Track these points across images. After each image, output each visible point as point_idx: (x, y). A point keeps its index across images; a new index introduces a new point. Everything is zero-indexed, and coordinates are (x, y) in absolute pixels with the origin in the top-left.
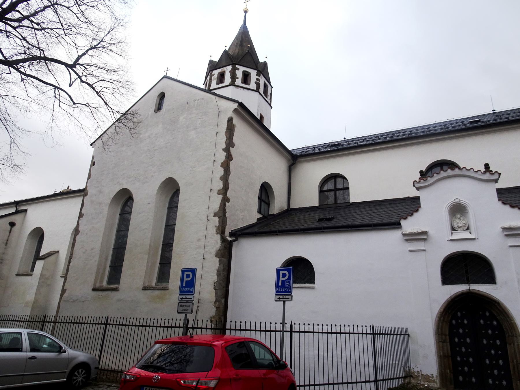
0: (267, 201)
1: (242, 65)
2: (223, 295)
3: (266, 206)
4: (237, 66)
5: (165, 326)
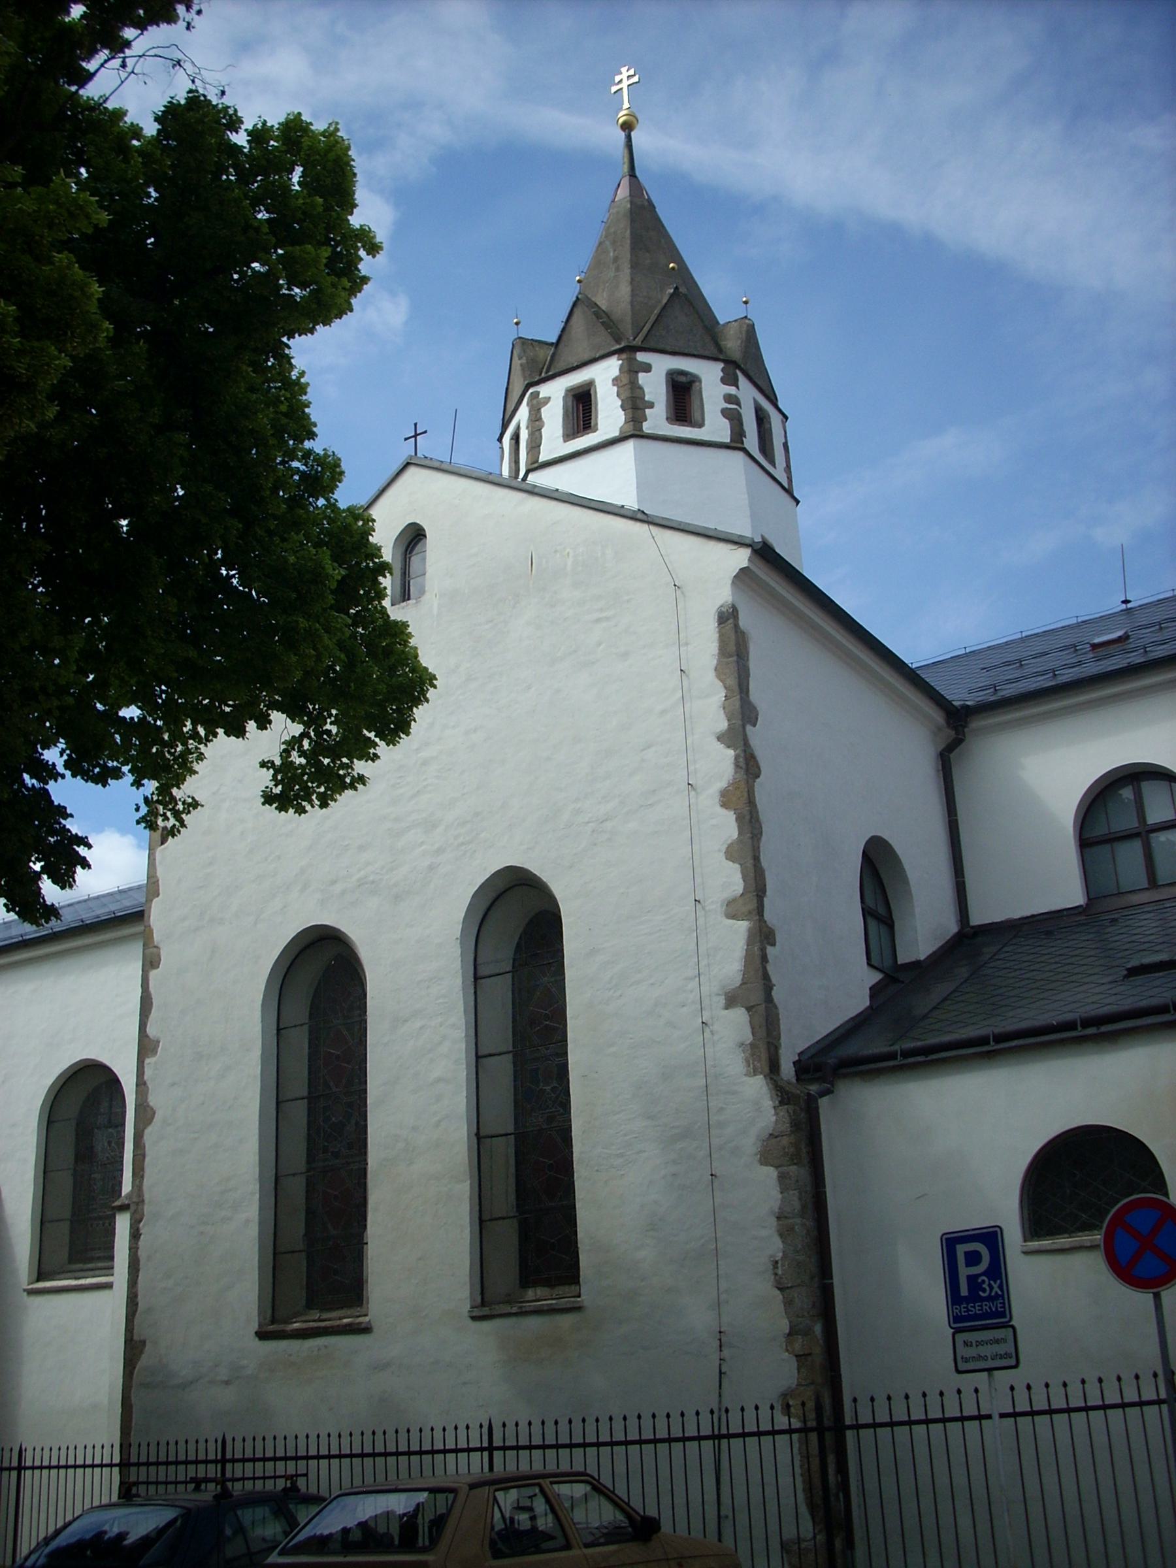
0: (882, 910)
1: (661, 346)
2: (814, 1306)
3: (884, 930)
4: (641, 357)
5: (310, 1454)
